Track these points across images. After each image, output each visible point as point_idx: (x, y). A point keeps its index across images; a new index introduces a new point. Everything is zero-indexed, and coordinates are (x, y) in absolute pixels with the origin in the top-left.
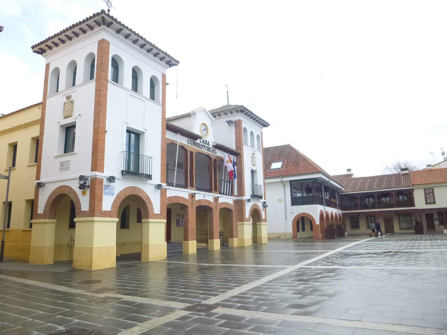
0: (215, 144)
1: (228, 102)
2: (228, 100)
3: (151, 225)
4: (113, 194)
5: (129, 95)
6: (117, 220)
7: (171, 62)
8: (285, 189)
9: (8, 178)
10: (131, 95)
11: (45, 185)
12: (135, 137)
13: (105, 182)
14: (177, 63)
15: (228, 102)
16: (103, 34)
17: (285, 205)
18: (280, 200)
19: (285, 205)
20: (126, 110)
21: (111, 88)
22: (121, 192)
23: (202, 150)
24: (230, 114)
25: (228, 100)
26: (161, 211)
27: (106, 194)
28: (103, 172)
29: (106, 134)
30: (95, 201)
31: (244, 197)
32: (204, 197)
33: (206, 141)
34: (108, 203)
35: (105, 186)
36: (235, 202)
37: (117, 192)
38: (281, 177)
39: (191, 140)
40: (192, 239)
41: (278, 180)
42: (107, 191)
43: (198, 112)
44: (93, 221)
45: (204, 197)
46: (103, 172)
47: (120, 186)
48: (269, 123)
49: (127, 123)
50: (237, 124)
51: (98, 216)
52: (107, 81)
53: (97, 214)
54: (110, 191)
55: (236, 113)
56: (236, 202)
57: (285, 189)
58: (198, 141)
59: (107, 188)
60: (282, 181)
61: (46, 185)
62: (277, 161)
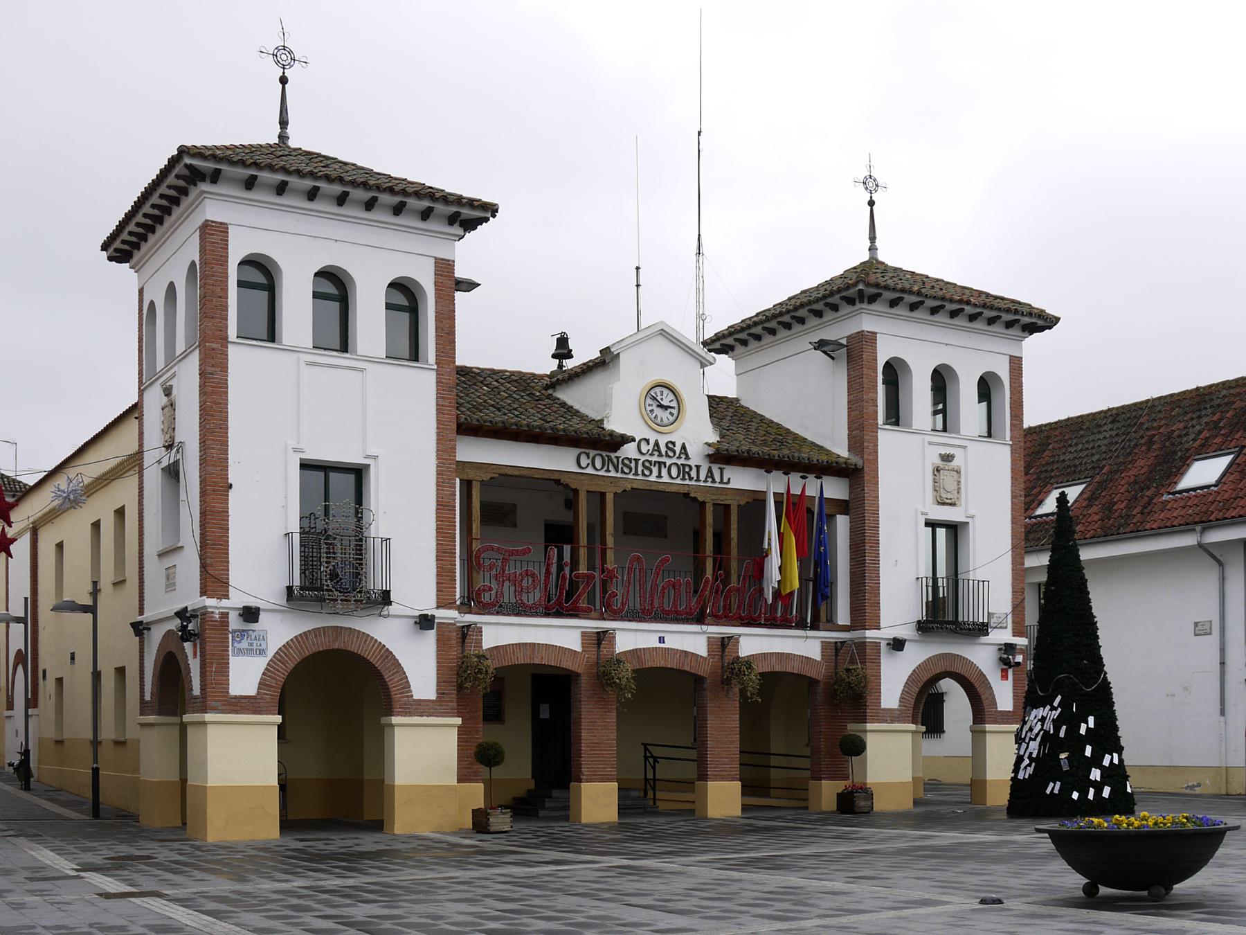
0: (711, 451)
1: (873, 249)
2: (873, 238)
3: (398, 732)
4: (262, 652)
5: (303, 365)
6: (278, 719)
7: (468, 214)
8: (1223, 580)
9: (91, 609)
10: (308, 364)
11: (149, 629)
12: (336, 491)
13: (235, 622)
14: (491, 210)
15: (873, 249)
16: (214, 206)
17: (1223, 650)
18: (1200, 630)
19: (1223, 650)
20: (297, 408)
21: (245, 362)
22: (287, 646)
23: (653, 478)
24: (813, 321)
25: (873, 238)
26: (440, 692)
27: (240, 652)
28: (227, 597)
29: (231, 493)
30: (217, 668)
31: (869, 633)
32: (662, 640)
33: (670, 445)
34: (245, 675)
35: (234, 631)
36: (837, 651)
37: (273, 647)
38: (1198, 528)
39: (592, 453)
40: (997, 783)
41: (1188, 540)
42: (244, 644)
43: (630, 346)
44: (204, 723)
45: (662, 640)
46: (227, 597)
47: (279, 631)
48: (1051, 310)
49: (296, 451)
50: (856, 353)
51: (215, 710)
52: (224, 341)
53: (214, 704)
54: (251, 644)
55: (849, 309)
56: (835, 650)
57: (1223, 580)
58: (629, 450)
59: (243, 636)
60: (1200, 545)
61: (153, 628)
62: (1205, 451)
